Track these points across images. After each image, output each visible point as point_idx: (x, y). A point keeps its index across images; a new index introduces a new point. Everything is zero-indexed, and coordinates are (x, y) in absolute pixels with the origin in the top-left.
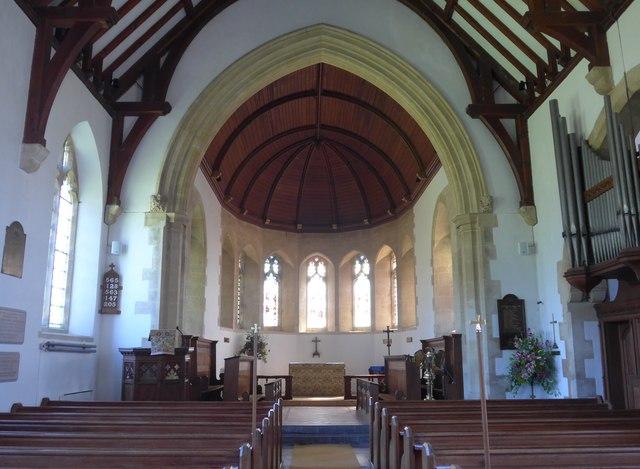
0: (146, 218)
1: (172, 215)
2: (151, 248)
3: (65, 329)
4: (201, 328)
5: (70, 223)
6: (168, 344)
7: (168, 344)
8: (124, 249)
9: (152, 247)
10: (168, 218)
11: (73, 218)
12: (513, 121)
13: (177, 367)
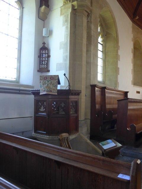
0: (61, 11)
1: (75, 3)
2: (64, 28)
3: (17, 82)
4: (116, 83)
5: (19, 20)
6: (51, 86)
7: (51, 86)
8: (50, 33)
9: (64, 27)
10: (73, 6)
11: (20, 17)
12: (137, 162)
13: (54, 106)
